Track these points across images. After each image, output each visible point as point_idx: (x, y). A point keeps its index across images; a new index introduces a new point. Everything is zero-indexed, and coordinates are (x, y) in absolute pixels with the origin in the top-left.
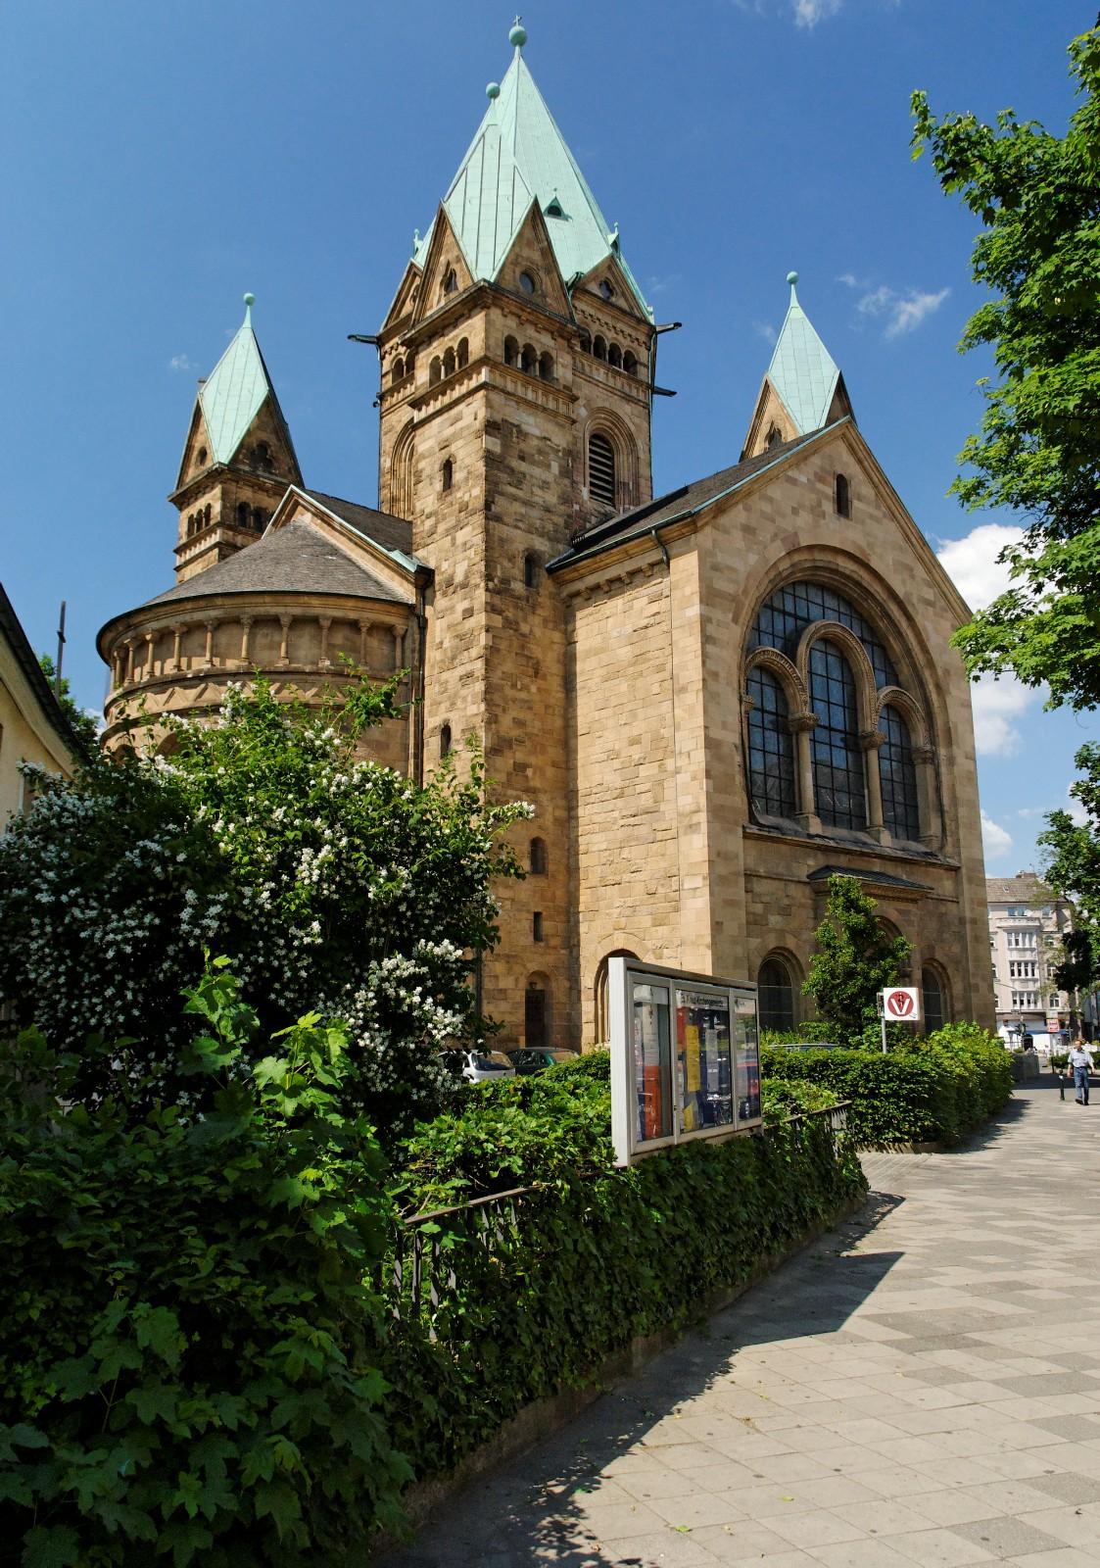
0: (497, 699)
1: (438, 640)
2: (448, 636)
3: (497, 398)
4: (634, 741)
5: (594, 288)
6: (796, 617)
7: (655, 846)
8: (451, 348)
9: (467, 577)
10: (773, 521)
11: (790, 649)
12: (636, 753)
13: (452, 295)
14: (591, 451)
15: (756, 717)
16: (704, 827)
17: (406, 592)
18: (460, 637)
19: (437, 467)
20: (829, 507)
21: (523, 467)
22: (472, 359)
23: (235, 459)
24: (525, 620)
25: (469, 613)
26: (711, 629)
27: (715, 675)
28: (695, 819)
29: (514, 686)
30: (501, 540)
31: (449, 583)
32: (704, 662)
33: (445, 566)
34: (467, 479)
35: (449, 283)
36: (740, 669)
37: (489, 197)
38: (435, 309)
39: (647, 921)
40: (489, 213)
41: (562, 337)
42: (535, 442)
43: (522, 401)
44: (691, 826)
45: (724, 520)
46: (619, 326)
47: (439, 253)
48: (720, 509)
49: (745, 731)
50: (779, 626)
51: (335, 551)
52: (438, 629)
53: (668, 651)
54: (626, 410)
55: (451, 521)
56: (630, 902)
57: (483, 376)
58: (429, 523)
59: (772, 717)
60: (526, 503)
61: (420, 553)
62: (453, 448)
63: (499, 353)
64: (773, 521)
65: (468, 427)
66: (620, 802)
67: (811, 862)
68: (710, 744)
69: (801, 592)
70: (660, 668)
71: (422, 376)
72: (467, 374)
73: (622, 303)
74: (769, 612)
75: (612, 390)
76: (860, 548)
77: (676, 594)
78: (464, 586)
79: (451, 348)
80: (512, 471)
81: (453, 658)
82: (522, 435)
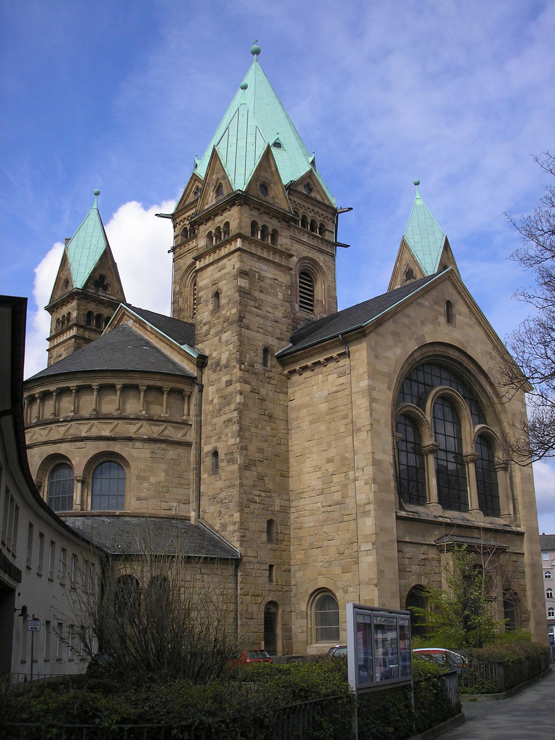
0: (247, 434)
1: (210, 399)
2: (217, 396)
3: (247, 258)
4: (330, 461)
5: (301, 189)
6: (425, 384)
7: (342, 524)
8: (219, 227)
9: (228, 361)
10: (410, 328)
11: (421, 404)
12: (331, 467)
13: (220, 198)
14: (300, 282)
15: (403, 447)
16: (372, 513)
17: (190, 369)
18: (224, 397)
19: (210, 296)
20: (442, 319)
21: (262, 296)
22: (232, 234)
23: (86, 286)
24: (263, 387)
25: (229, 383)
26: (375, 394)
27: (378, 421)
28: (367, 508)
29: (257, 427)
30: (249, 339)
31: (218, 364)
32: (371, 414)
33: (215, 354)
34: (228, 303)
35: (219, 189)
36: (392, 417)
37: (241, 143)
38: (210, 205)
39: (338, 570)
40: (241, 152)
41: (283, 220)
42: (269, 281)
43: (261, 258)
44: (365, 512)
45: (382, 329)
46: (316, 209)
47: (212, 174)
48: (380, 323)
49: (396, 454)
50: (415, 390)
51: (148, 344)
52: (210, 392)
53: (349, 407)
54: (320, 258)
55: (219, 328)
56: (327, 558)
57: (239, 243)
58: (205, 328)
59: (412, 445)
60: (264, 317)
61: (199, 346)
62: (220, 285)
63: (247, 231)
64: (410, 328)
65: (229, 273)
66: (321, 498)
67: (436, 533)
68: (376, 463)
69: (427, 369)
70: (345, 417)
71: (202, 243)
72: (229, 242)
73: (319, 198)
74: (409, 381)
75: (312, 247)
76: (462, 344)
77: (354, 373)
78: (226, 366)
79: (219, 227)
80: (255, 300)
81: (220, 410)
82: (261, 279)
